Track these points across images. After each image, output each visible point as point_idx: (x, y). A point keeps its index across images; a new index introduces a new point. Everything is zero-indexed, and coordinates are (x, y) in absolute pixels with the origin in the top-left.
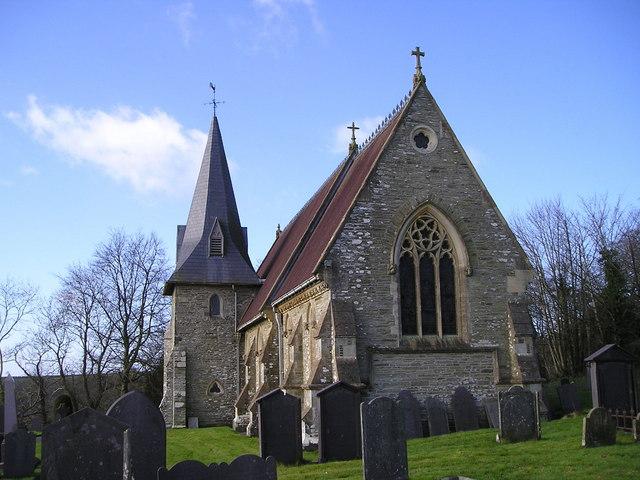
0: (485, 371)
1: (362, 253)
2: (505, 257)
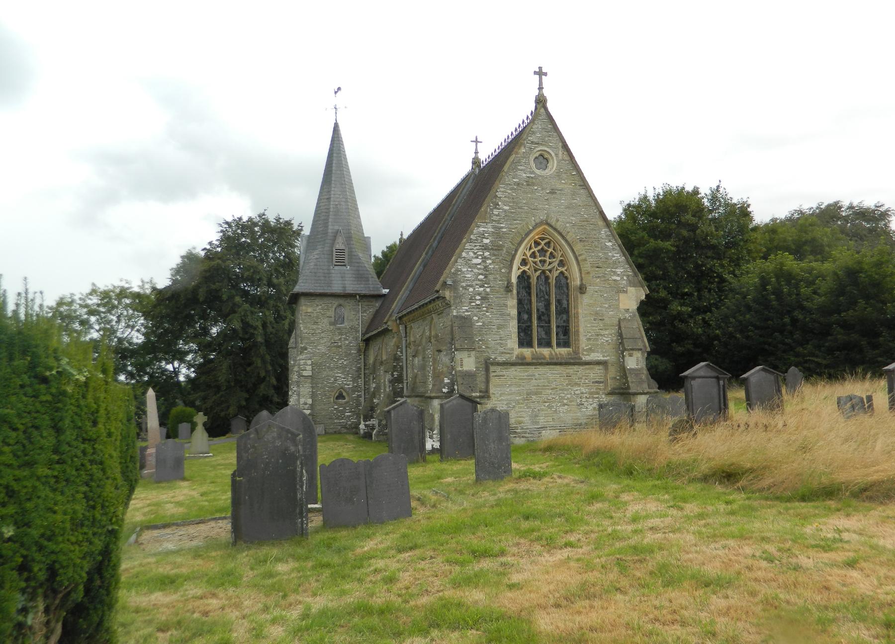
1: (480, 272)
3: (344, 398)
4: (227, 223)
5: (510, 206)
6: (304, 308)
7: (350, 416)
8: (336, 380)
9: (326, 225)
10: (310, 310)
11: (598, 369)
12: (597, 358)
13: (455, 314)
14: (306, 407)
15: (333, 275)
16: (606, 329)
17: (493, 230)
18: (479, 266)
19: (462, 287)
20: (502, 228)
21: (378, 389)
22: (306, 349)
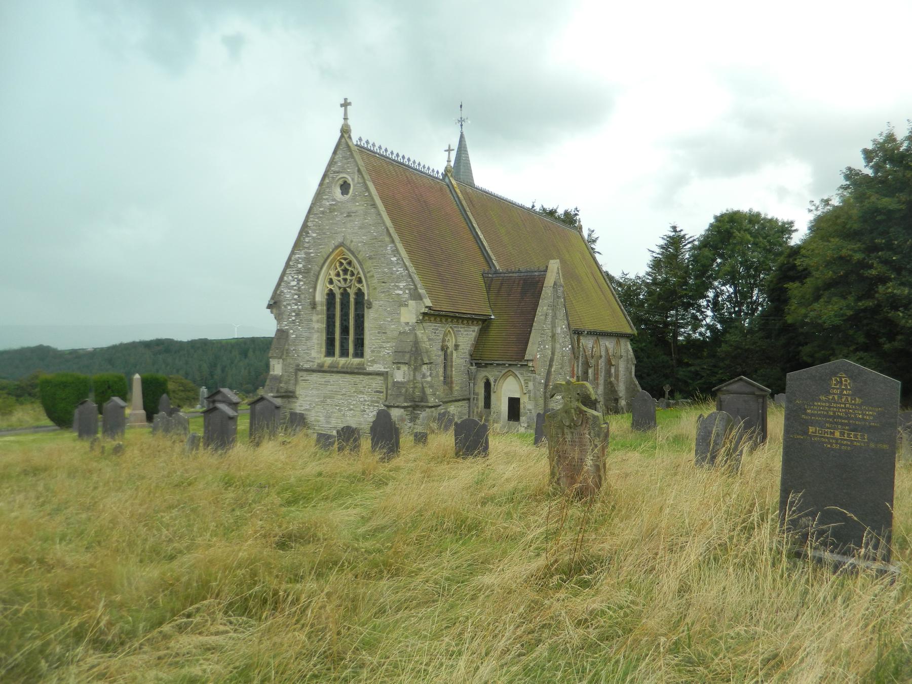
0: (377, 392)
2: (401, 289)
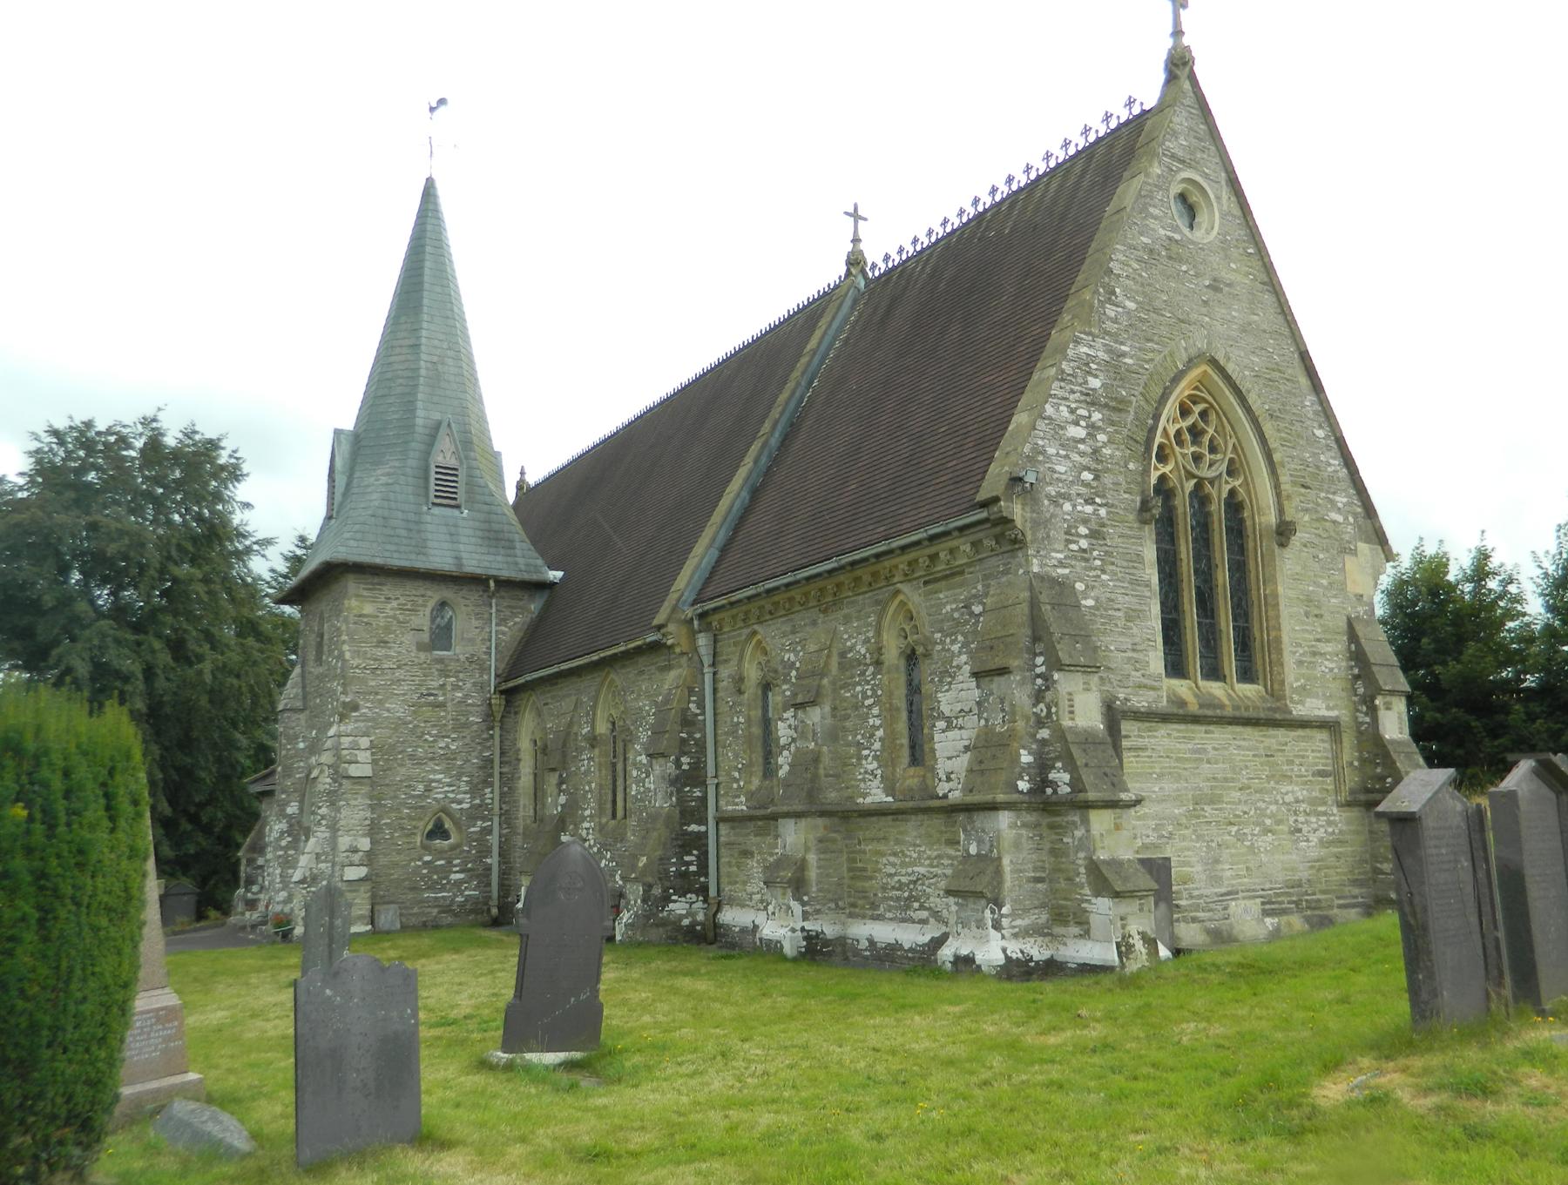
1: (1085, 461)
3: (445, 835)
4: (55, 433)
5: (1137, 302)
6: (354, 603)
7: (461, 882)
8: (428, 789)
9: (409, 407)
10: (368, 609)
11: (1320, 738)
12: (1317, 713)
13: (1036, 569)
14: (356, 858)
15: (429, 527)
16: (1328, 641)
17: (1106, 357)
18: (1081, 447)
19: (1048, 497)
20: (1124, 355)
21: (572, 807)
22: (356, 708)
